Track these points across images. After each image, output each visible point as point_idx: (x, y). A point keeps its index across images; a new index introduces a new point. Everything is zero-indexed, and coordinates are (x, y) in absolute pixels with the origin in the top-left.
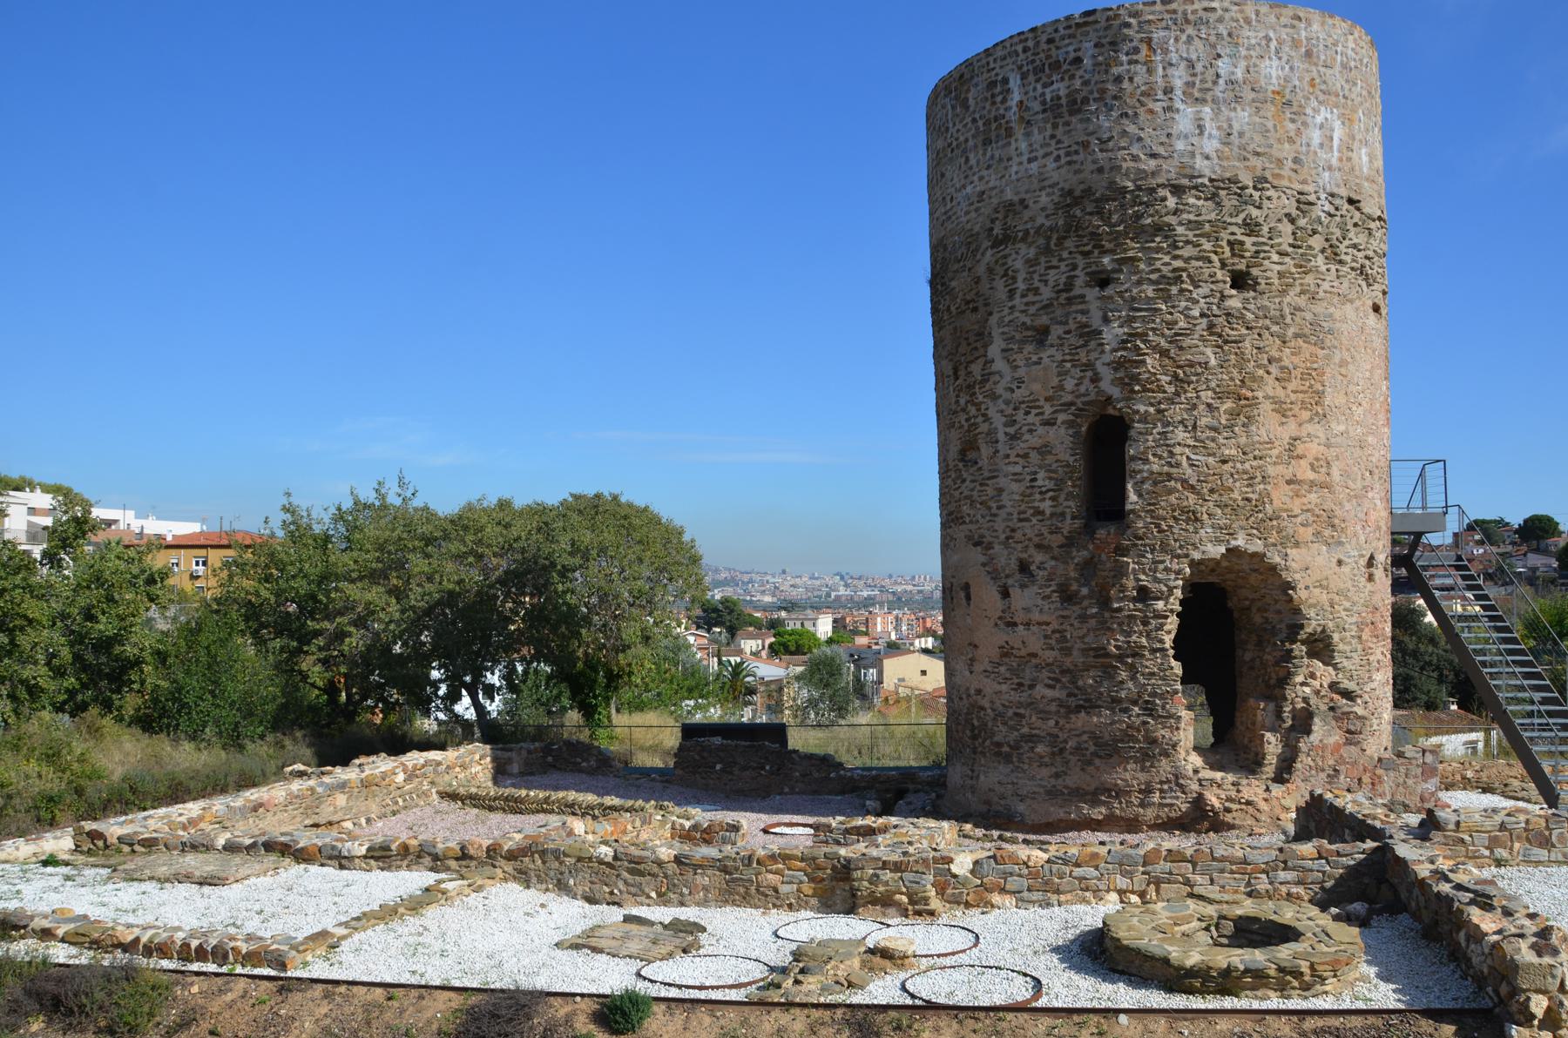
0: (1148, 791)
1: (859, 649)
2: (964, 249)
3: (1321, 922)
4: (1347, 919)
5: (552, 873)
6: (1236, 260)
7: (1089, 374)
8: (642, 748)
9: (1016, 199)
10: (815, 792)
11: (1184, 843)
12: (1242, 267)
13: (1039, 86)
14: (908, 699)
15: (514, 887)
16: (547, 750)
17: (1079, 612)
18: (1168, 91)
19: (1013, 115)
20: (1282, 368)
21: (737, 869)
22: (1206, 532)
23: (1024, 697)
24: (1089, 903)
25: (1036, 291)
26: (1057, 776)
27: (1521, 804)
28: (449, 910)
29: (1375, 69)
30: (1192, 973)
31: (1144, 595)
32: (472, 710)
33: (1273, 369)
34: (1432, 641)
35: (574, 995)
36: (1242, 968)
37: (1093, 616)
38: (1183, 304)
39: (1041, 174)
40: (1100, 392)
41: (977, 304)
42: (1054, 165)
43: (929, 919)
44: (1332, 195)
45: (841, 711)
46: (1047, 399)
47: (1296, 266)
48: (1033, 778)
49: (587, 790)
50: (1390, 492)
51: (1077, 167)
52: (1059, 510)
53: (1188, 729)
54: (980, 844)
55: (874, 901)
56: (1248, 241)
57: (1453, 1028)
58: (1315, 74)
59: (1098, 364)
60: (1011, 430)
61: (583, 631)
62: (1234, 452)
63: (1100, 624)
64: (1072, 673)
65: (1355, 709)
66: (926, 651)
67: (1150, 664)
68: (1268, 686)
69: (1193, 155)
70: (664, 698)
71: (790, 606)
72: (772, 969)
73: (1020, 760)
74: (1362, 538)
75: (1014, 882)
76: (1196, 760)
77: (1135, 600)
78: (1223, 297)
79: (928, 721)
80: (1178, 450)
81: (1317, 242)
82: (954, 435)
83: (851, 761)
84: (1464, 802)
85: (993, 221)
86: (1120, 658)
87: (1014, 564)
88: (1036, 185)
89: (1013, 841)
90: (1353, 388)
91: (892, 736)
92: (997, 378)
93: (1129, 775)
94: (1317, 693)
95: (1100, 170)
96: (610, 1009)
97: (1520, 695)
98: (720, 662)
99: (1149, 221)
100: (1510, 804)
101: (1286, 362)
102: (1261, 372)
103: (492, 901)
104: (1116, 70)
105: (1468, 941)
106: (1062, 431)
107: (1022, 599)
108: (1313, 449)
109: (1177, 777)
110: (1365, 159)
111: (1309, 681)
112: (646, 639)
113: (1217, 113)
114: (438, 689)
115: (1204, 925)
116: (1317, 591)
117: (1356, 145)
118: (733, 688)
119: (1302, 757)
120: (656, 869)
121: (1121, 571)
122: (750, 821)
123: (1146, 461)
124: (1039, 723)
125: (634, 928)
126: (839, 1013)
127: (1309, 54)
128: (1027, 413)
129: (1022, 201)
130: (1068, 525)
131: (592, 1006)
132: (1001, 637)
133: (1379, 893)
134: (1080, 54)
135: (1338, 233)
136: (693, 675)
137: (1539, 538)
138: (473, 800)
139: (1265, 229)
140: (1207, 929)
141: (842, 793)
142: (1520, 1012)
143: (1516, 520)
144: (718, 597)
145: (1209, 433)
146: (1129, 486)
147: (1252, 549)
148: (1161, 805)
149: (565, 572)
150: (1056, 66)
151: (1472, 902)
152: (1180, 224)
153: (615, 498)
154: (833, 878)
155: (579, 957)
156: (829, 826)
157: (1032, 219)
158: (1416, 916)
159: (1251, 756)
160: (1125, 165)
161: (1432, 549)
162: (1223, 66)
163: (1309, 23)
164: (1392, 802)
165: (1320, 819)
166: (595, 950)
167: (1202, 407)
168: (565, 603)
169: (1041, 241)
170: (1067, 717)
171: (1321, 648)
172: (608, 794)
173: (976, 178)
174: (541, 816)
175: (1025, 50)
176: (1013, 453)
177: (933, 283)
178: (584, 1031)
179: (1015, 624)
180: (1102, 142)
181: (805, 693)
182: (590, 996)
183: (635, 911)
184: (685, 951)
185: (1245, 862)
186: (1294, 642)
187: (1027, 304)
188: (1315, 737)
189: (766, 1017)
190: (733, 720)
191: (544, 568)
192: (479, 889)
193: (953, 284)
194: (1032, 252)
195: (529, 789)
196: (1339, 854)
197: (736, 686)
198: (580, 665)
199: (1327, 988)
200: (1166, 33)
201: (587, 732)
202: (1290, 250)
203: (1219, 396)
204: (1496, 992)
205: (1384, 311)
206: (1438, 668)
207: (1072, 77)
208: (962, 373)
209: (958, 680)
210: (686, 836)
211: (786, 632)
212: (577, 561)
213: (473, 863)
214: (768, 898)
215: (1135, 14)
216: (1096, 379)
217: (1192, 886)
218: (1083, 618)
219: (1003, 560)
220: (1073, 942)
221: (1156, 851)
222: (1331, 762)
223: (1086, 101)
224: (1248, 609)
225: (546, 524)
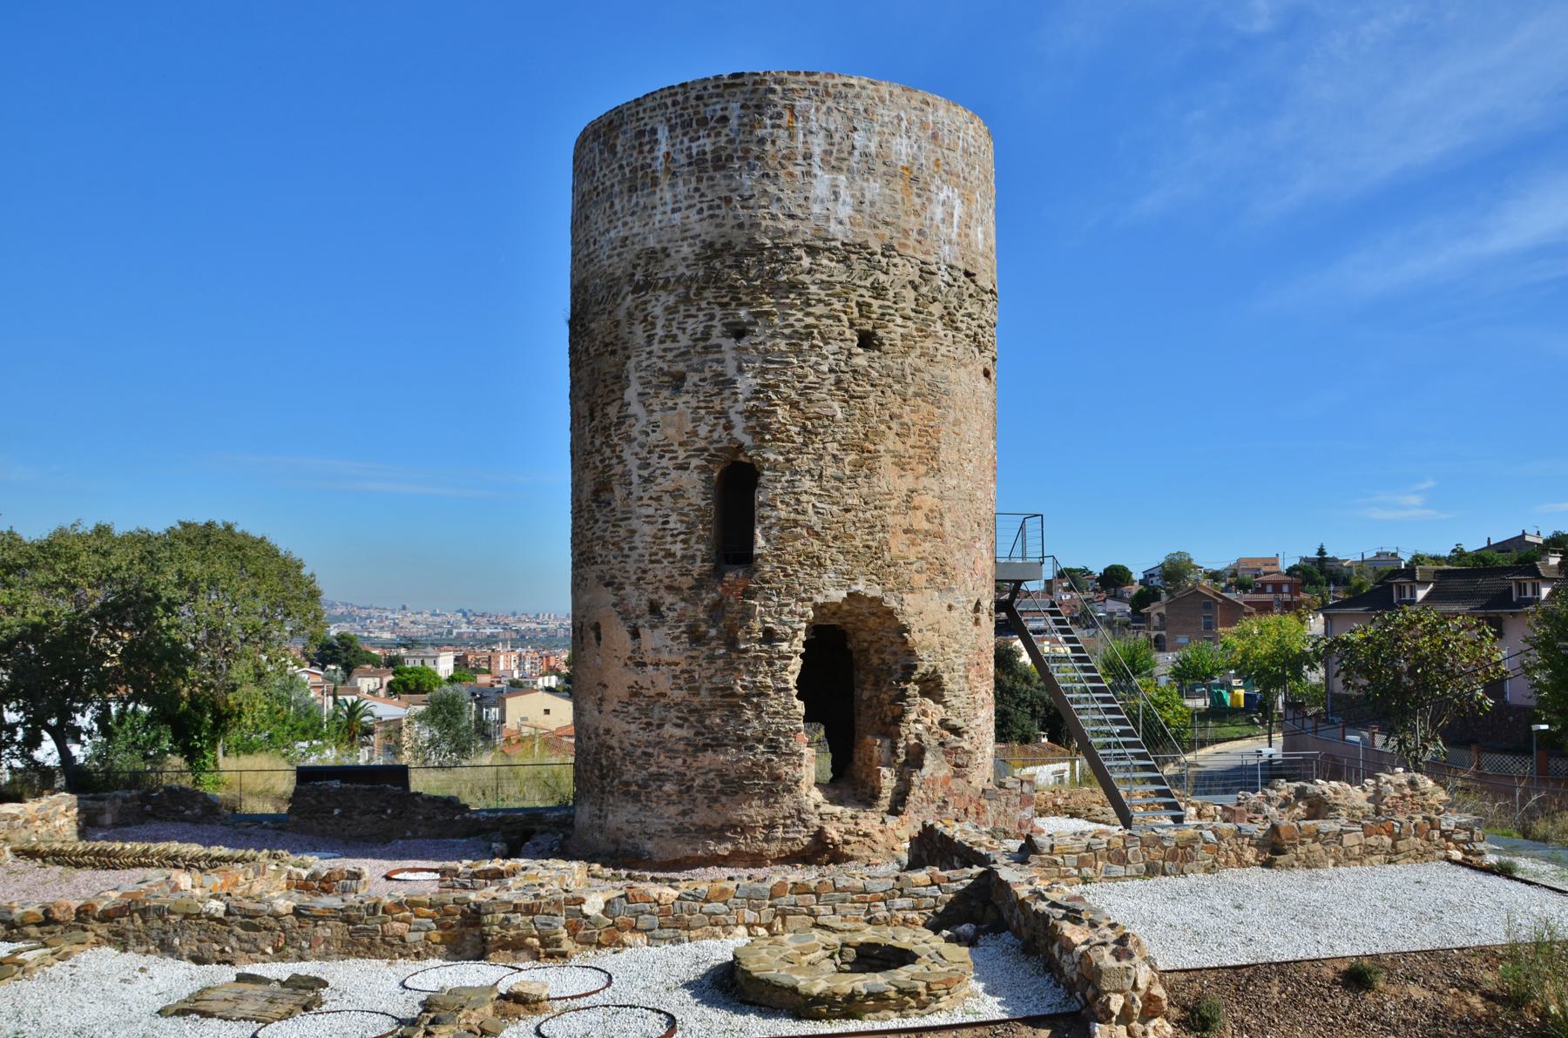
0: (771, 826)
1: (482, 689)
2: (604, 292)
3: (934, 944)
4: (957, 939)
5: (154, 933)
6: (863, 321)
7: (723, 421)
8: (251, 794)
9: (658, 247)
10: (439, 836)
11: (808, 875)
12: (869, 327)
13: (686, 140)
14: (532, 738)
15: (109, 951)
16: (146, 798)
18: (807, 156)
19: (659, 165)
20: (902, 424)
21: (361, 919)
22: (829, 577)
23: (652, 736)
24: (718, 937)
25: (674, 338)
26: (684, 813)
27: (1102, 826)
28: (26, 984)
29: (991, 157)
30: (819, 999)
31: (769, 636)
32: (56, 754)
33: (894, 425)
34: (1027, 679)
36: (865, 992)
37: (720, 657)
38: (814, 359)
39: (683, 224)
41: (617, 348)
42: (697, 217)
43: (561, 962)
44: (952, 267)
45: (462, 749)
46: (681, 444)
47: (918, 330)
48: (660, 817)
49: (192, 840)
50: (995, 542)
51: (719, 221)
52: (690, 552)
53: (810, 764)
54: (609, 884)
55: (504, 945)
56: (876, 303)
58: (939, 155)
59: (732, 412)
60: (645, 473)
61: (189, 669)
62: (856, 501)
63: (728, 664)
66: (549, 690)
67: (774, 703)
68: (884, 723)
69: (828, 218)
70: (276, 739)
71: (411, 643)
72: (401, 1022)
73: (648, 799)
75: (644, 921)
76: (817, 795)
77: (761, 641)
78: (850, 355)
79: (553, 760)
81: (936, 309)
82: (588, 475)
83: (476, 803)
84: (1054, 827)
85: (635, 267)
86: (746, 698)
87: (644, 605)
88: (678, 235)
89: (642, 879)
90: (964, 446)
91: (517, 776)
92: (633, 421)
93: (753, 811)
94: (929, 729)
95: (741, 226)
97: (1102, 728)
98: (336, 702)
99: (784, 278)
100: (1093, 826)
101: (906, 419)
102: (883, 427)
104: (759, 132)
105: (1061, 952)
106: (695, 475)
107: (653, 639)
108: (928, 501)
109: (799, 812)
110: (980, 236)
111: (921, 718)
112: (260, 676)
113: (851, 181)
114: (15, 733)
115: (828, 953)
116: (929, 634)
117: (973, 224)
118: (349, 728)
119: (915, 790)
120: (272, 923)
121: (748, 614)
122: (372, 868)
123: (774, 507)
124: (667, 762)
125: (248, 988)
127: (934, 136)
128: (661, 457)
129: (664, 250)
130: (698, 568)
132: (630, 677)
133: (983, 913)
134: (726, 113)
135: (955, 302)
136: (307, 715)
137: (1117, 586)
138: (58, 857)
139: (891, 294)
140: (831, 957)
141: (467, 835)
142: (1102, 1011)
143: (1097, 569)
145: (834, 483)
146: (758, 531)
147: (871, 593)
148: (785, 840)
149: (169, 607)
150: (703, 122)
151: (1065, 917)
152: (814, 283)
153: (229, 528)
154: (462, 924)
157: (673, 268)
159: (868, 790)
160: (764, 223)
161: (1028, 594)
162: (859, 139)
163: (936, 109)
164: (994, 830)
165: (931, 848)
166: (205, 1014)
167: (828, 458)
168: (170, 639)
169: (681, 290)
170: (694, 756)
171: (933, 687)
172: (214, 843)
173: (620, 223)
174: (139, 870)
175: (675, 103)
176: (646, 495)
177: (572, 324)
179: (645, 665)
180: (744, 199)
181: (426, 734)
183: (249, 969)
184: (306, 1009)
185: (865, 892)
186: (907, 681)
187: (665, 350)
188: (926, 771)
190: (347, 762)
192: (66, 957)
193: (593, 325)
194: (672, 300)
195: (124, 841)
196: (949, 880)
197: (352, 727)
198: (184, 705)
199: (941, 1005)
200: (808, 102)
201: (190, 777)
202: (912, 314)
203: (844, 448)
204: (1083, 996)
205: (993, 377)
206: (1031, 704)
207: (718, 134)
208: (598, 414)
209: (586, 719)
210: (303, 886)
211: (406, 670)
214: (394, 948)
215: (781, 82)
216: (729, 427)
217: (816, 917)
218: (711, 659)
219: (633, 601)
220: (704, 976)
221: (782, 884)
222: (941, 794)
223: (730, 158)
224: (867, 650)
225: (150, 553)
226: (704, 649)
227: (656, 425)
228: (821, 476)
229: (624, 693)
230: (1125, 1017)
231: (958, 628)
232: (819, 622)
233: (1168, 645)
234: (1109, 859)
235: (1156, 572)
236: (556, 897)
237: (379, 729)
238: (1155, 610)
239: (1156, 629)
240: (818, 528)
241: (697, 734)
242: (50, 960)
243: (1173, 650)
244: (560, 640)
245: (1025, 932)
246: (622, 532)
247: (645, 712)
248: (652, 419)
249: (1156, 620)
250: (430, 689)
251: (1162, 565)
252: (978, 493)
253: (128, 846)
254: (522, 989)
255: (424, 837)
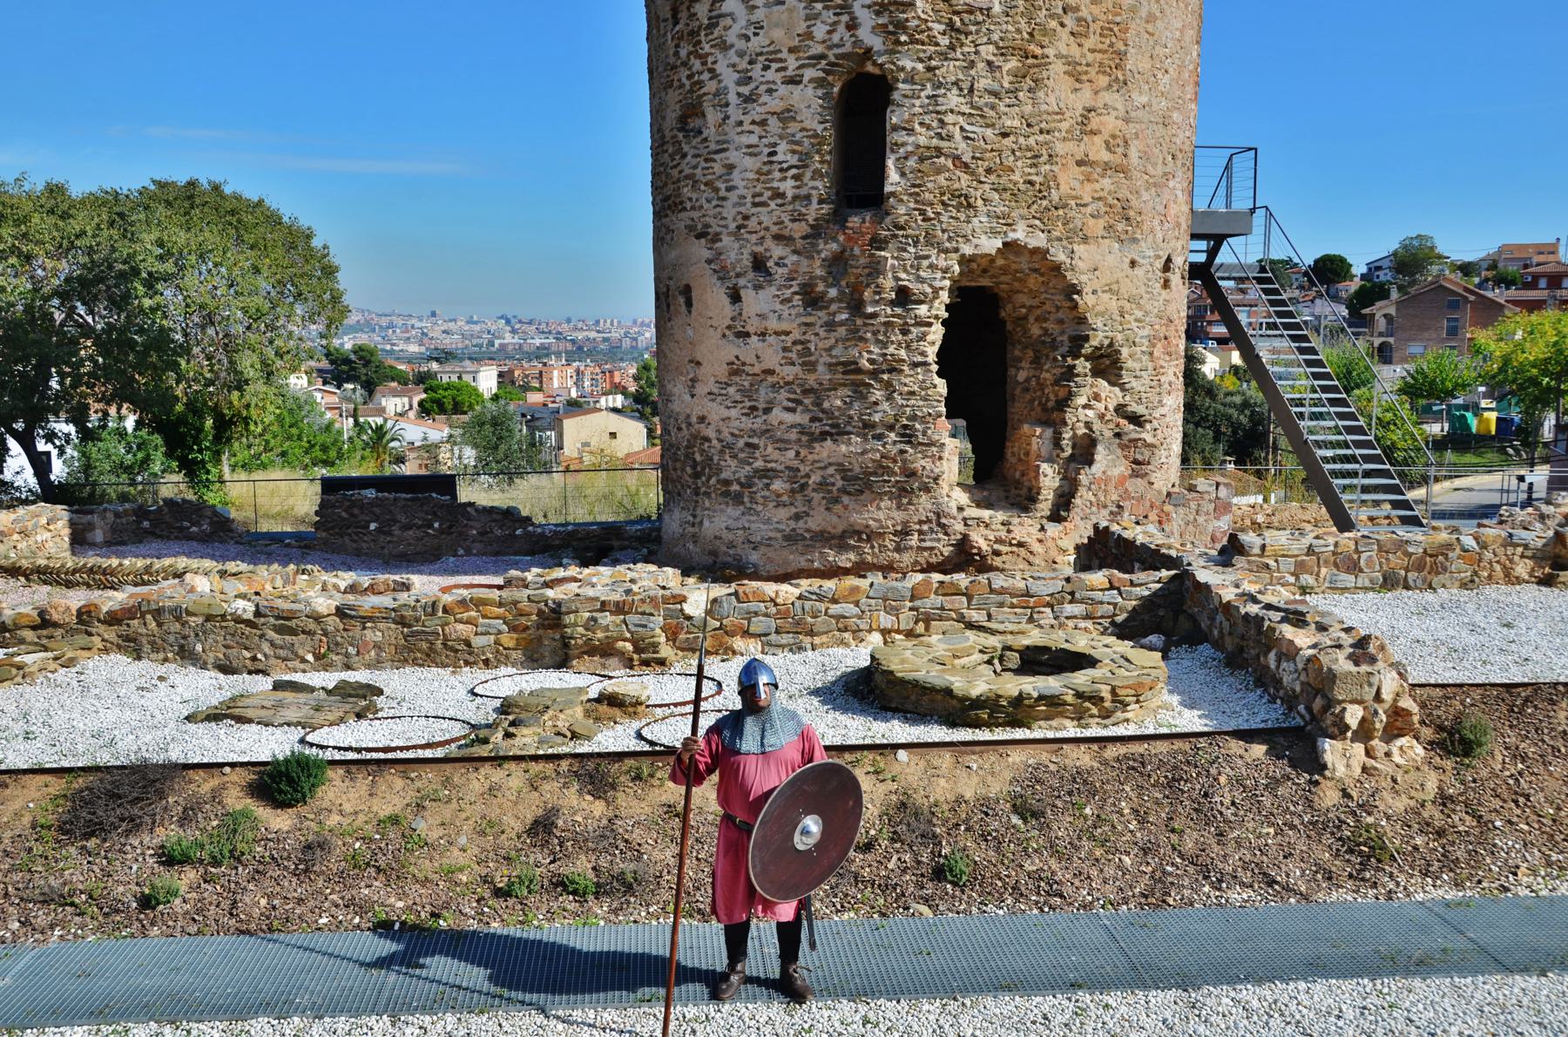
0: (905, 533)
5: (171, 638)
7: (845, 18)
8: (267, 516)
10: (497, 554)
17: (826, 318)
20: (1079, 20)
21: (417, 620)
22: (980, 221)
23: (758, 423)
24: (847, 645)
26: (797, 517)
28: (28, 689)
30: (978, 703)
31: (904, 297)
33: (1069, 20)
35: (221, 765)
36: (1035, 695)
37: (842, 324)
40: (857, 42)
46: (791, 50)
48: (768, 521)
52: (804, 191)
53: (950, 455)
55: (591, 650)
57: (1264, 748)
60: (745, 90)
61: (183, 363)
62: (1016, 123)
64: (817, 394)
65: (1143, 436)
66: (615, 410)
67: (909, 380)
68: (1045, 409)
70: (291, 457)
71: (444, 356)
74: (1160, 235)
76: (961, 497)
77: (892, 303)
80: (949, 118)
82: (673, 96)
86: (874, 374)
87: (747, 261)
90: (1159, 51)
92: (728, 21)
93: (882, 514)
94: (1101, 417)
96: (270, 776)
98: (357, 423)
101: (1084, 13)
102: (1053, 24)
103: (90, 676)
105: (1279, 661)
106: (810, 91)
107: (757, 302)
109: (938, 515)
111: (1092, 403)
115: (986, 657)
116: (1106, 296)
119: (1082, 491)
120: (312, 625)
121: (876, 269)
123: (911, 131)
124: (776, 455)
125: (289, 696)
126: (565, 765)
128: (766, 68)
130: (814, 211)
131: (249, 776)
132: (730, 350)
133: (1176, 617)
140: (990, 662)
144: (348, 346)
146: (890, 163)
149: (151, 283)
153: (216, 188)
155: (222, 730)
156: (524, 580)
158: (1218, 645)
159: (1024, 492)
165: (1104, 550)
166: (241, 720)
167: (981, 65)
170: (809, 446)
171: (1108, 365)
176: (747, 119)
178: (238, 807)
179: (748, 335)
182: (242, 764)
185: (1028, 594)
186: (1076, 356)
188: (1097, 469)
189: (473, 775)
191: (122, 275)
196: (1132, 584)
198: (179, 408)
203: (1002, 52)
204: (1309, 709)
208: (683, 15)
211: (439, 387)
212: (169, 267)
213: (59, 632)
214: (458, 654)
216: (852, 26)
218: (831, 326)
219: (733, 256)
220: (833, 683)
222: (1115, 497)
224: (1025, 318)
225: (121, 215)
226: (820, 314)
227: (759, 26)
228: (971, 90)
229: (722, 371)
230: (1364, 733)
231: (1142, 290)
232: (965, 283)
233: (1396, 356)
234: (1336, 565)
235: (1386, 263)
236: (652, 593)
237: (412, 455)
238: (1380, 310)
239: (1381, 335)
240: (966, 158)
241: (813, 420)
242: (52, 665)
243: (1404, 360)
244: (626, 352)
245: (1229, 644)
246: (718, 168)
247: (748, 393)
248: (754, 18)
249: (1381, 324)
250: (471, 407)
251: (1395, 254)
252: (1175, 115)
253: (126, 562)
254: (616, 689)
255: (480, 554)
